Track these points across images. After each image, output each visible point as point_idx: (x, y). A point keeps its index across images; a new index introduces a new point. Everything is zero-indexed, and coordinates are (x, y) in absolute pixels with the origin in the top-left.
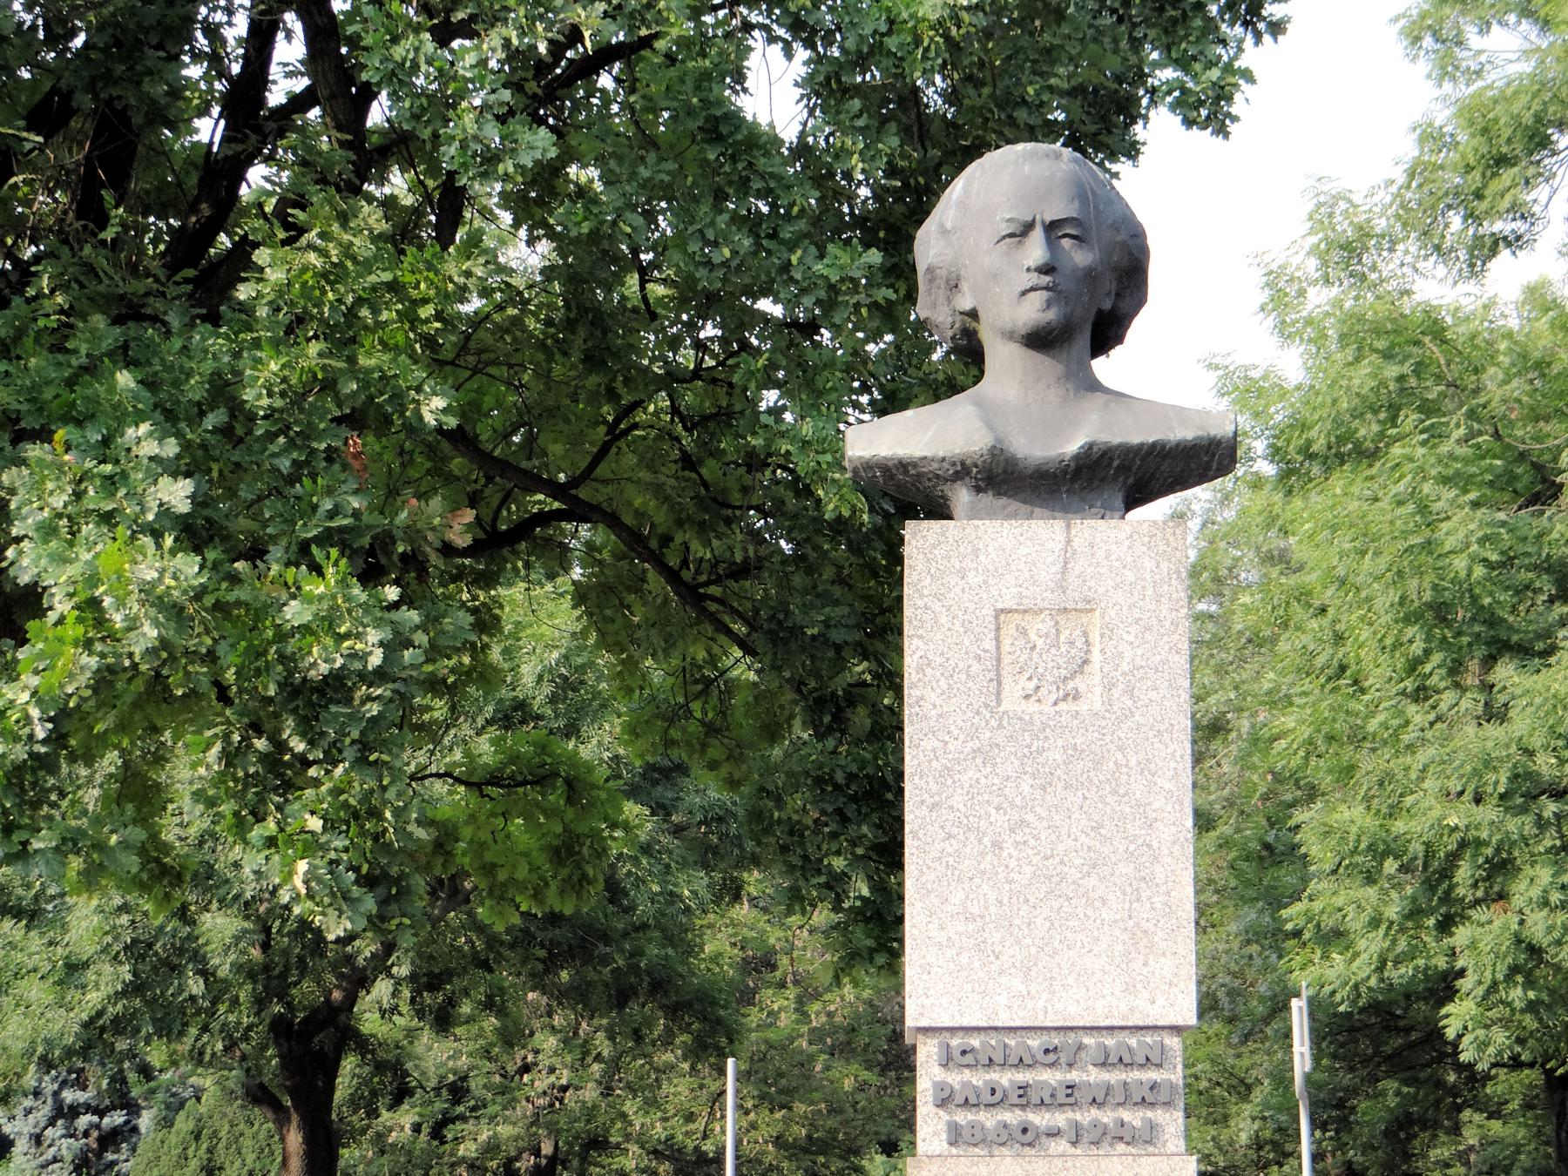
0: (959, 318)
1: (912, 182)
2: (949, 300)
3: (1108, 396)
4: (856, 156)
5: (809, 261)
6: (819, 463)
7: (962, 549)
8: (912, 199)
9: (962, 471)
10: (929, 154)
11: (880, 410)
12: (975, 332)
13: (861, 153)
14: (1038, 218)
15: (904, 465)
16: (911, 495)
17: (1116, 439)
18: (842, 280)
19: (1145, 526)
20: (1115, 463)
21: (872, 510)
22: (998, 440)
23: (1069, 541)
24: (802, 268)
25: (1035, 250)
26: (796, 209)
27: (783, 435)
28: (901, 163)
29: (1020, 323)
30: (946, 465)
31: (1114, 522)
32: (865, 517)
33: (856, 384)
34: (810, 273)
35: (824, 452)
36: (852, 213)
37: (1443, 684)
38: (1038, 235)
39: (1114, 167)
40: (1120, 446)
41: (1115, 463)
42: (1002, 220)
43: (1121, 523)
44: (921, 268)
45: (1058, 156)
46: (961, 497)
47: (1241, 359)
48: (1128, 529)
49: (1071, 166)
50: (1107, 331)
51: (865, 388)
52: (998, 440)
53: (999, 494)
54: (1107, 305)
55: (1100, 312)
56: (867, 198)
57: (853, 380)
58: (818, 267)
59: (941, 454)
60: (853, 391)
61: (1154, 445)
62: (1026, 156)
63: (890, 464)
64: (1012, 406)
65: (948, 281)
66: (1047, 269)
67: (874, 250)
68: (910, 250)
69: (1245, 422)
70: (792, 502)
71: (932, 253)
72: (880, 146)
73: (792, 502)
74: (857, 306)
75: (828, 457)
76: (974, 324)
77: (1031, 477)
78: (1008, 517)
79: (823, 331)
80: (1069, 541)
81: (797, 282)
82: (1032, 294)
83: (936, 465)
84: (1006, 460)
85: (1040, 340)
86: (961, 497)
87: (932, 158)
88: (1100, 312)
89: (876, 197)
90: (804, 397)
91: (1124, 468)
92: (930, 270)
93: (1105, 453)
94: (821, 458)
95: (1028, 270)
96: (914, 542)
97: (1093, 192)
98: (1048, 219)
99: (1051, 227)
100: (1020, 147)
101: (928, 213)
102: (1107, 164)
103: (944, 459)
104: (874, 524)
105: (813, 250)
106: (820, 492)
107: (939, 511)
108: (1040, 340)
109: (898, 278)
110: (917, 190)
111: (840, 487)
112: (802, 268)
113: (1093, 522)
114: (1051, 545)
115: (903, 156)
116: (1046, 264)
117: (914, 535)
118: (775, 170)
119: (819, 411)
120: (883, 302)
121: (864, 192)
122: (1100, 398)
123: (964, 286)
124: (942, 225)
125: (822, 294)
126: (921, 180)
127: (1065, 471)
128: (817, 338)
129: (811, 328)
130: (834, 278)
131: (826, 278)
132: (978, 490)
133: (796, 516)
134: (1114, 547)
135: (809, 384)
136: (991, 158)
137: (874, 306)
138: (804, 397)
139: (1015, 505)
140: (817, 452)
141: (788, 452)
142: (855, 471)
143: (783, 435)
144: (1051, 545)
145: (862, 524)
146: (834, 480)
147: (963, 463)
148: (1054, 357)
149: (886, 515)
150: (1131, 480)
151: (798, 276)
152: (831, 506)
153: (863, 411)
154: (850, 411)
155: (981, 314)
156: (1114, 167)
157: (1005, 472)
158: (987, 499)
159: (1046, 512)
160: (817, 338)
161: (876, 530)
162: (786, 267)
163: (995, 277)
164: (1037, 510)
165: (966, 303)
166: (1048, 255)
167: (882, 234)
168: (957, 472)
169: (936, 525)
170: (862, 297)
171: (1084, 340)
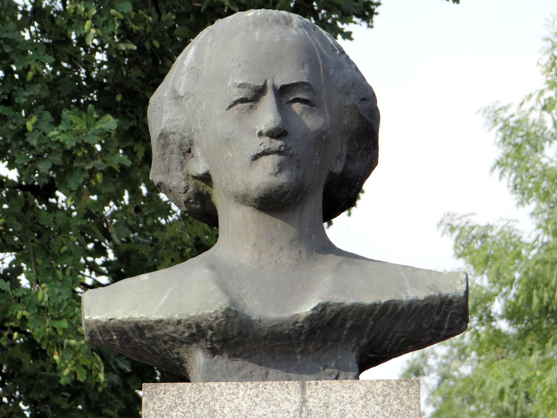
0: (192, 182)
1: (147, 45)
2: (182, 164)
3: (340, 259)
4: (89, 23)
5: (44, 126)
6: (55, 329)
7: (198, 411)
8: (152, 63)
9: (197, 333)
10: (164, 17)
11: (117, 275)
12: (208, 196)
13: (94, 19)
14: (269, 83)
15: (139, 328)
16: (151, 356)
17: (350, 301)
18: (78, 146)
19: (379, 385)
20: (348, 325)
21: (108, 370)
22: (233, 302)
23: (304, 402)
24: (38, 134)
25: (267, 115)
26: (30, 75)
27: (19, 300)
28: (135, 28)
29: (253, 187)
30: (181, 328)
31: (348, 383)
32: (102, 377)
33: (90, 246)
34: (45, 139)
35: (60, 318)
36: (88, 78)
37: (168, 221)
38: (268, 101)
39: (347, 28)
40: (353, 306)
41: (348, 325)
42: (234, 85)
43: (355, 383)
44: (154, 132)
45: (288, 22)
46: (197, 359)
47: (480, 220)
48: (362, 389)
49: (301, 31)
50: (341, 195)
51: (100, 251)
52: (233, 302)
53: (234, 356)
54: (338, 168)
55: (331, 175)
56: (103, 63)
57: (88, 241)
58: (53, 133)
59: (177, 317)
60: (89, 253)
61: (386, 305)
62: (257, 23)
63: (126, 327)
64: (243, 269)
65: (181, 146)
66: (276, 134)
67: (109, 117)
68: (145, 114)
69: (482, 281)
70: (28, 363)
71: (165, 118)
72: (113, 11)
73: (28, 363)
74: (92, 172)
75: (64, 324)
76: (207, 188)
77: (265, 338)
78: (243, 379)
79: (58, 193)
80: (304, 402)
81: (33, 148)
82: (264, 159)
83: (171, 328)
84: (241, 322)
85: (271, 203)
86: (197, 359)
87: (167, 21)
88: (331, 175)
89: (111, 61)
90: (39, 261)
91: (357, 329)
92: (163, 135)
93: (338, 314)
94: (57, 324)
95: (260, 134)
96: (151, 405)
97: (323, 56)
98: (279, 83)
99: (282, 92)
100: (251, 13)
101: (162, 77)
102: (339, 24)
103: (179, 322)
104: (111, 383)
105: (48, 116)
106: (56, 357)
107: (177, 374)
108: (271, 203)
109: (136, 140)
110: (153, 55)
111: (76, 353)
112: (38, 134)
113: (327, 383)
114: (286, 405)
115: (136, 21)
116: (277, 129)
117: (151, 398)
118: (10, 36)
119: (55, 275)
120: (117, 168)
121: (100, 57)
122: (332, 260)
123: (197, 151)
124: (174, 91)
125: (58, 159)
126: (157, 44)
127: (299, 332)
128: (53, 200)
129: (47, 191)
130: (70, 144)
131: (62, 144)
132: (213, 352)
133: (33, 377)
134: (348, 407)
135: (47, 251)
136: (221, 25)
137: (109, 173)
138: (39, 261)
139: (250, 366)
140: (53, 318)
141: (24, 318)
142: (92, 334)
143: (19, 300)
144: (286, 405)
145: (98, 384)
146: (70, 347)
147: (198, 326)
148: (286, 221)
149: (124, 375)
150: (364, 341)
151: (34, 143)
152: (66, 372)
153: (100, 273)
154: (87, 272)
155: (215, 179)
156: (347, 28)
157: (240, 334)
158: (222, 361)
159: (281, 373)
160: (53, 200)
161: (114, 389)
162: (22, 133)
163: (227, 141)
164: (272, 371)
165: (199, 167)
166: (279, 119)
167: (119, 98)
168: (192, 335)
169: (173, 388)
170: (98, 163)
171: (316, 203)
